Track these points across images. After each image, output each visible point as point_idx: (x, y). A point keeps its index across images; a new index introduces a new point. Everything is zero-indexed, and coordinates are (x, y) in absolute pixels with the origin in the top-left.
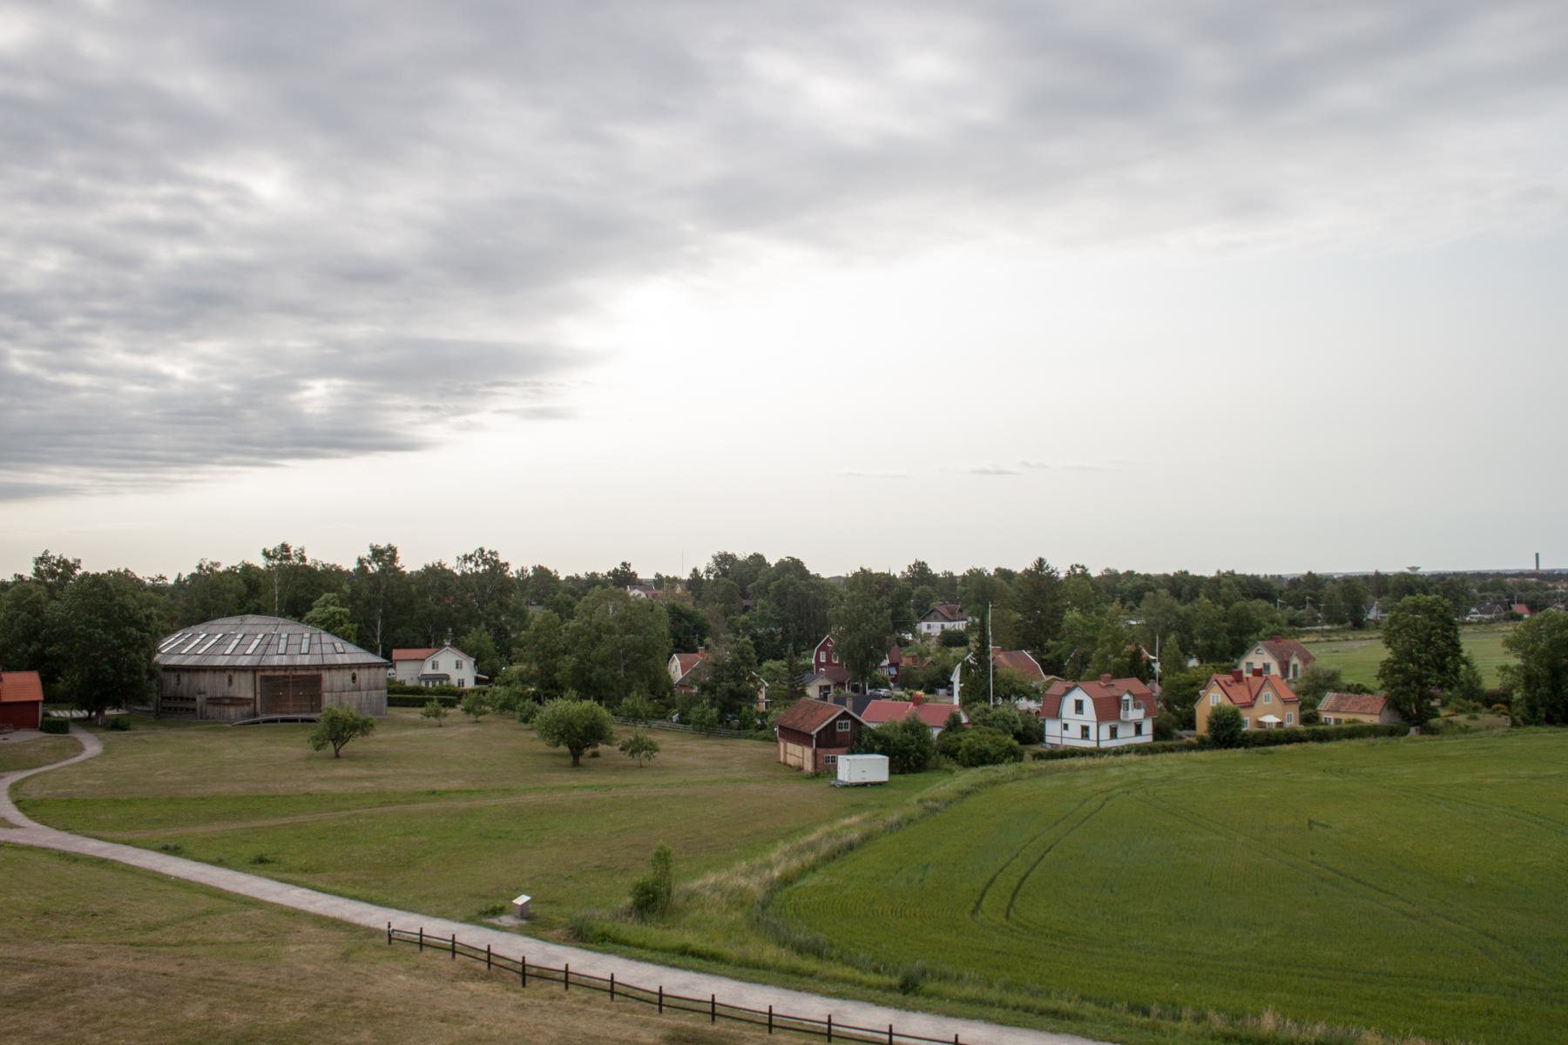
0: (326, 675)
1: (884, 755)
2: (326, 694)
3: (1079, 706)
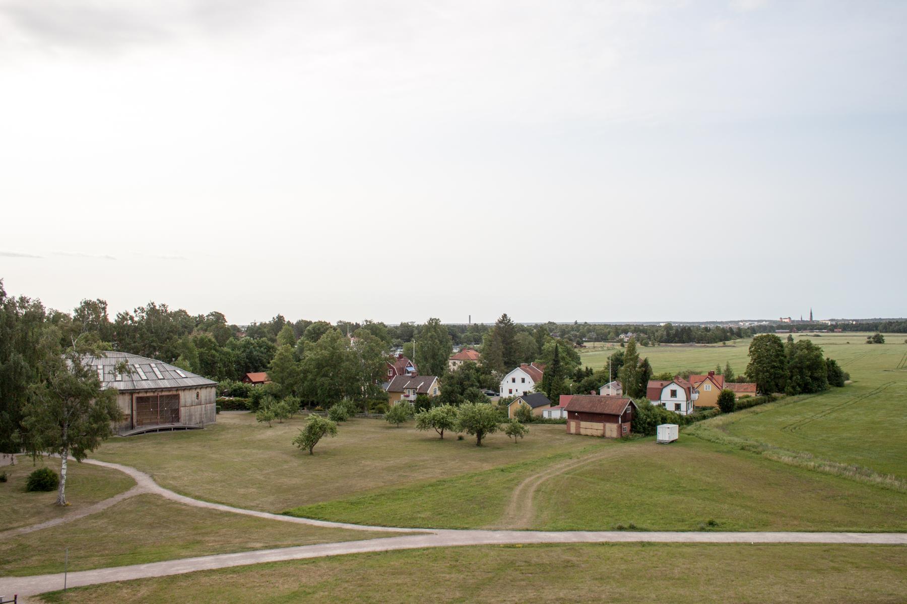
0: (181, 394)
1: (674, 423)
2: (182, 408)
3: (674, 394)
